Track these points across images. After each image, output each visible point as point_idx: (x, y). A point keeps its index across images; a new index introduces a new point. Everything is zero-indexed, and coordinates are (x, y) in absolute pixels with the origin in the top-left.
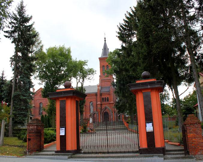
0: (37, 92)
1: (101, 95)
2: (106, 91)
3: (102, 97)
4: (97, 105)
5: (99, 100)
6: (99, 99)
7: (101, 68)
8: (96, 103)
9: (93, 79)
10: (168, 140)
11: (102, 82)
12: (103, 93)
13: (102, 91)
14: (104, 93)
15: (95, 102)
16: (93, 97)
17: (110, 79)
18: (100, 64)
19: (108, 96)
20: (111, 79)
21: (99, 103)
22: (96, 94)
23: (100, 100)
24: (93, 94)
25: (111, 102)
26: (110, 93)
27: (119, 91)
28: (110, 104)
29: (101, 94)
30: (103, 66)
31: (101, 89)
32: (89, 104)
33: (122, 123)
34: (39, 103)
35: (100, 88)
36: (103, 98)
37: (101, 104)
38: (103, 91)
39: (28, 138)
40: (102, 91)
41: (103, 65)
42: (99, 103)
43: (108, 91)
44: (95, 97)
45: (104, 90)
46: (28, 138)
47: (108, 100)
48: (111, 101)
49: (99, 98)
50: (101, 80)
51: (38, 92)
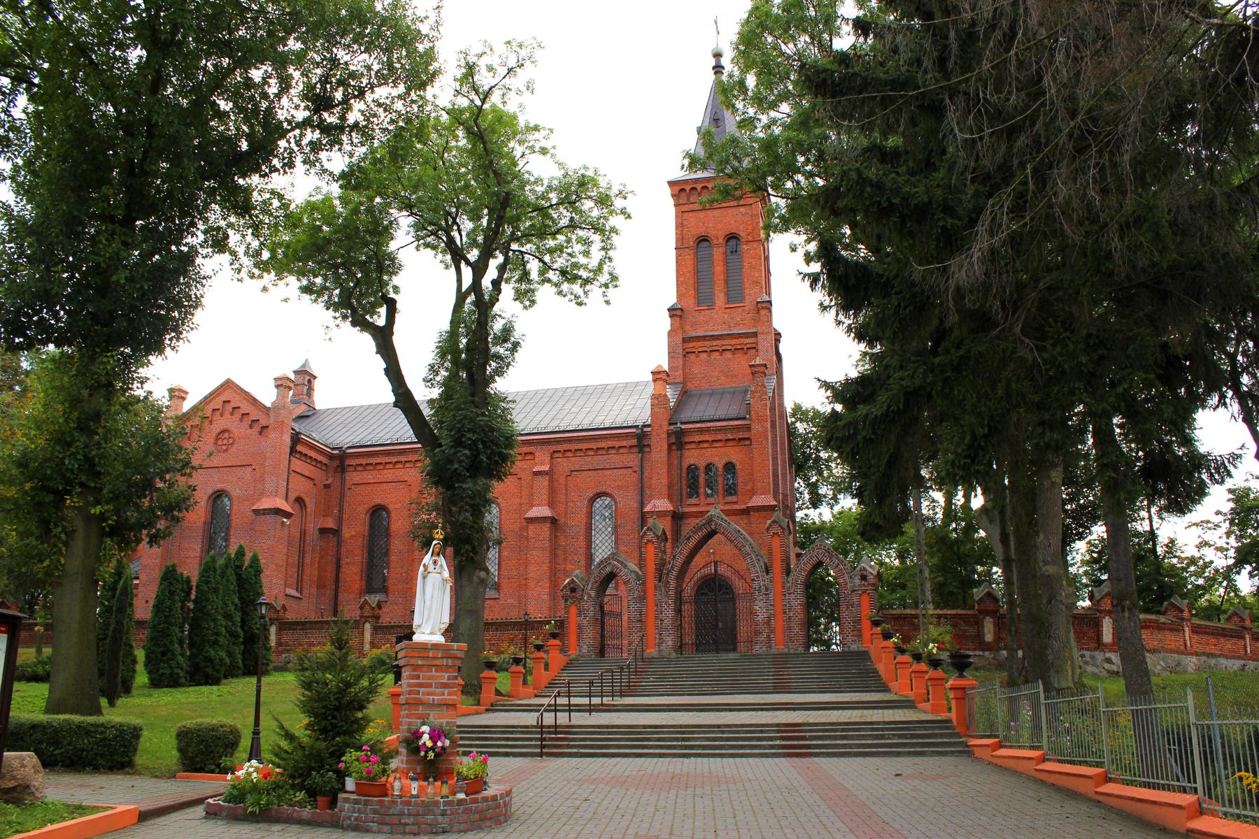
0: (195, 409)
1: (678, 441)
2: (721, 413)
3: (686, 464)
4: (643, 517)
5: (664, 481)
6: (659, 475)
7: (689, 258)
8: (635, 505)
9: (604, 278)
10: (1100, 770)
11: (686, 354)
12: (689, 432)
13: (686, 415)
14: (701, 431)
15: (628, 501)
16: (615, 459)
17: (747, 335)
18: (680, 226)
19: (734, 454)
20: (755, 335)
21: (661, 504)
22: (639, 438)
23: (670, 486)
24: (612, 436)
25: (758, 501)
26: (748, 428)
27: (669, 534)
28: (746, 512)
29: (682, 433)
30: (703, 239)
31: (680, 403)
32: (582, 517)
33: (855, 671)
34: (210, 491)
35: (671, 394)
36: (692, 470)
37: (677, 517)
38: (688, 414)
39: (669, 544)
40: (686, 415)
41: (701, 231)
42: (661, 504)
43: (491, 760)
44: (633, 459)
45: (699, 410)
46: (669, 544)
47: (731, 490)
48: (753, 493)
49: (664, 471)
50: (685, 340)
51: (217, 404)
